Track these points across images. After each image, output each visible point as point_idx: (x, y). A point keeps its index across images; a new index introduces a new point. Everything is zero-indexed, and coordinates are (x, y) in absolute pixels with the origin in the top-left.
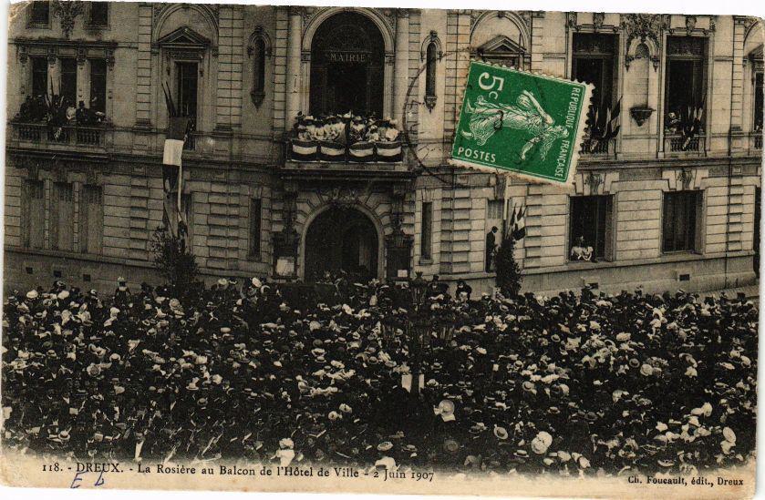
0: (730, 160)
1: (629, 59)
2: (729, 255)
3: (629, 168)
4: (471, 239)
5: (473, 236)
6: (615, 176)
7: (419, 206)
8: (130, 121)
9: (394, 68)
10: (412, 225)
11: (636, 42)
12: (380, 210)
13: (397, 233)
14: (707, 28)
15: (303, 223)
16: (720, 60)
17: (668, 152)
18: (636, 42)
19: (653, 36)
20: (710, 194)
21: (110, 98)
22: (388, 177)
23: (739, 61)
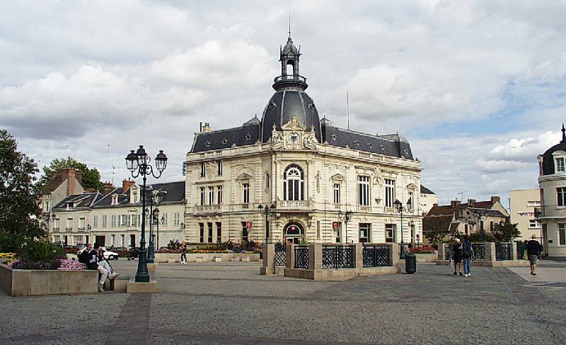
11: (375, 179)
12: (303, 221)
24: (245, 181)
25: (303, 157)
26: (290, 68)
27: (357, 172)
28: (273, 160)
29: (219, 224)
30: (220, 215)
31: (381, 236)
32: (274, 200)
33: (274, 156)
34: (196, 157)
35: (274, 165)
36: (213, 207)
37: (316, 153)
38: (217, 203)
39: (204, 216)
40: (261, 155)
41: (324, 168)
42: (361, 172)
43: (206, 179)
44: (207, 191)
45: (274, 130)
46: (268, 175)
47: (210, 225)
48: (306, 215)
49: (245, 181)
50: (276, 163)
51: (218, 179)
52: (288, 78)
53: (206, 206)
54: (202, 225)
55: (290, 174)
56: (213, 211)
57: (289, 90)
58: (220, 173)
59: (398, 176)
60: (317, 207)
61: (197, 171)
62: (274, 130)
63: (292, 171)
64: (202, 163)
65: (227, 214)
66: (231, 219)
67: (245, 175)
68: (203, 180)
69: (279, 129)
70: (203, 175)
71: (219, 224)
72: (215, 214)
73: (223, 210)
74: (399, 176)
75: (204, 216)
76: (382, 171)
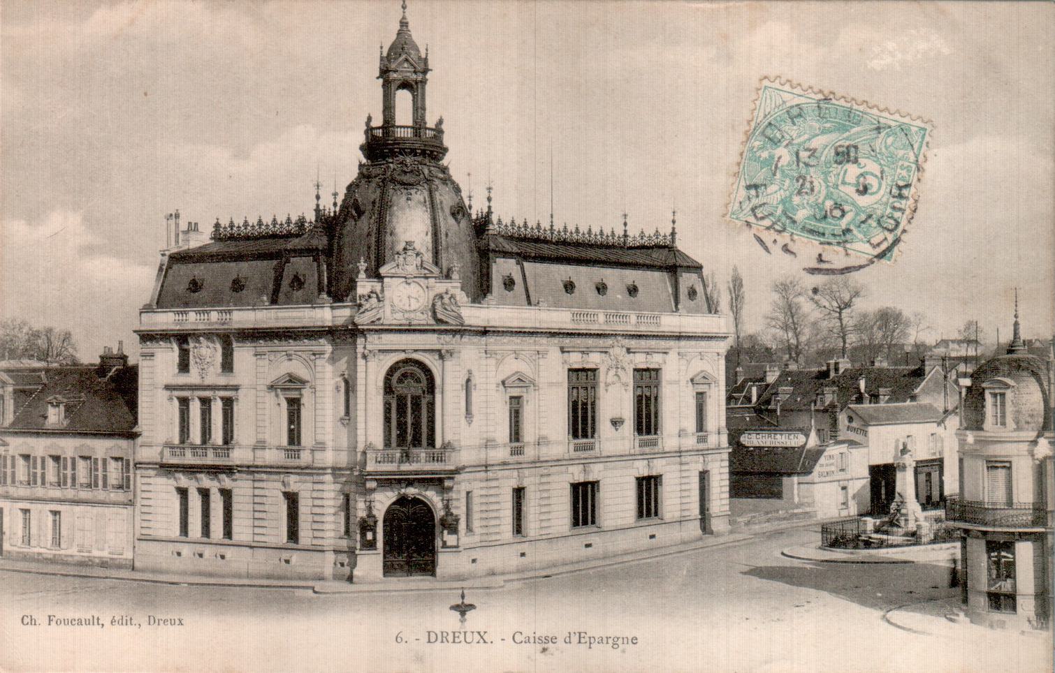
0: (680, 452)
1: (607, 385)
2: (682, 519)
3: (607, 459)
4: (501, 516)
5: (501, 514)
6: (601, 466)
7: (464, 495)
8: (737, 168)
9: (382, 286)
10: (458, 499)
11: (612, 372)
12: (432, 497)
13: (448, 513)
14: (661, 362)
15: (380, 512)
16: (670, 383)
17: (637, 448)
18: (612, 372)
19: (623, 368)
20: (668, 477)
21: (569, 287)
22: (381, 165)
23: (683, 383)
24: (292, 395)
25: (431, 340)
26: (403, 99)
27: (565, 362)
28: (360, 349)
29: (227, 494)
30: (229, 470)
31: (627, 507)
32: (361, 447)
33: (360, 341)
34: (165, 320)
35: (361, 362)
36: (210, 453)
37: (461, 331)
38: (220, 441)
39: (191, 470)
40: (331, 333)
41: (484, 362)
42: (576, 360)
43: (193, 377)
44: (195, 408)
45: (362, 275)
46: (346, 382)
47: (205, 494)
48: (437, 481)
49: (292, 395)
50: (364, 357)
51: (222, 381)
52: (400, 133)
53: (193, 447)
54: (183, 492)
55: (400, 381)
56: (210, 459)
57: (399, 156)
58: (227, 366)
59: (667, 357)
60: (464, 457)
61: (167, 356)
62: (362, 275)
63: (404, 375)
64: (182, 338)
65: (251, 470)
66: (257, 484)
67: (292, 379)
68: (183, 379)
69: (375, 274)
70: (184, 366)
71: (227, 494)
72: (214, 471)
73: (239, 456)
74: (673, 355)
75: (191, 470)
76: (629, 351)
